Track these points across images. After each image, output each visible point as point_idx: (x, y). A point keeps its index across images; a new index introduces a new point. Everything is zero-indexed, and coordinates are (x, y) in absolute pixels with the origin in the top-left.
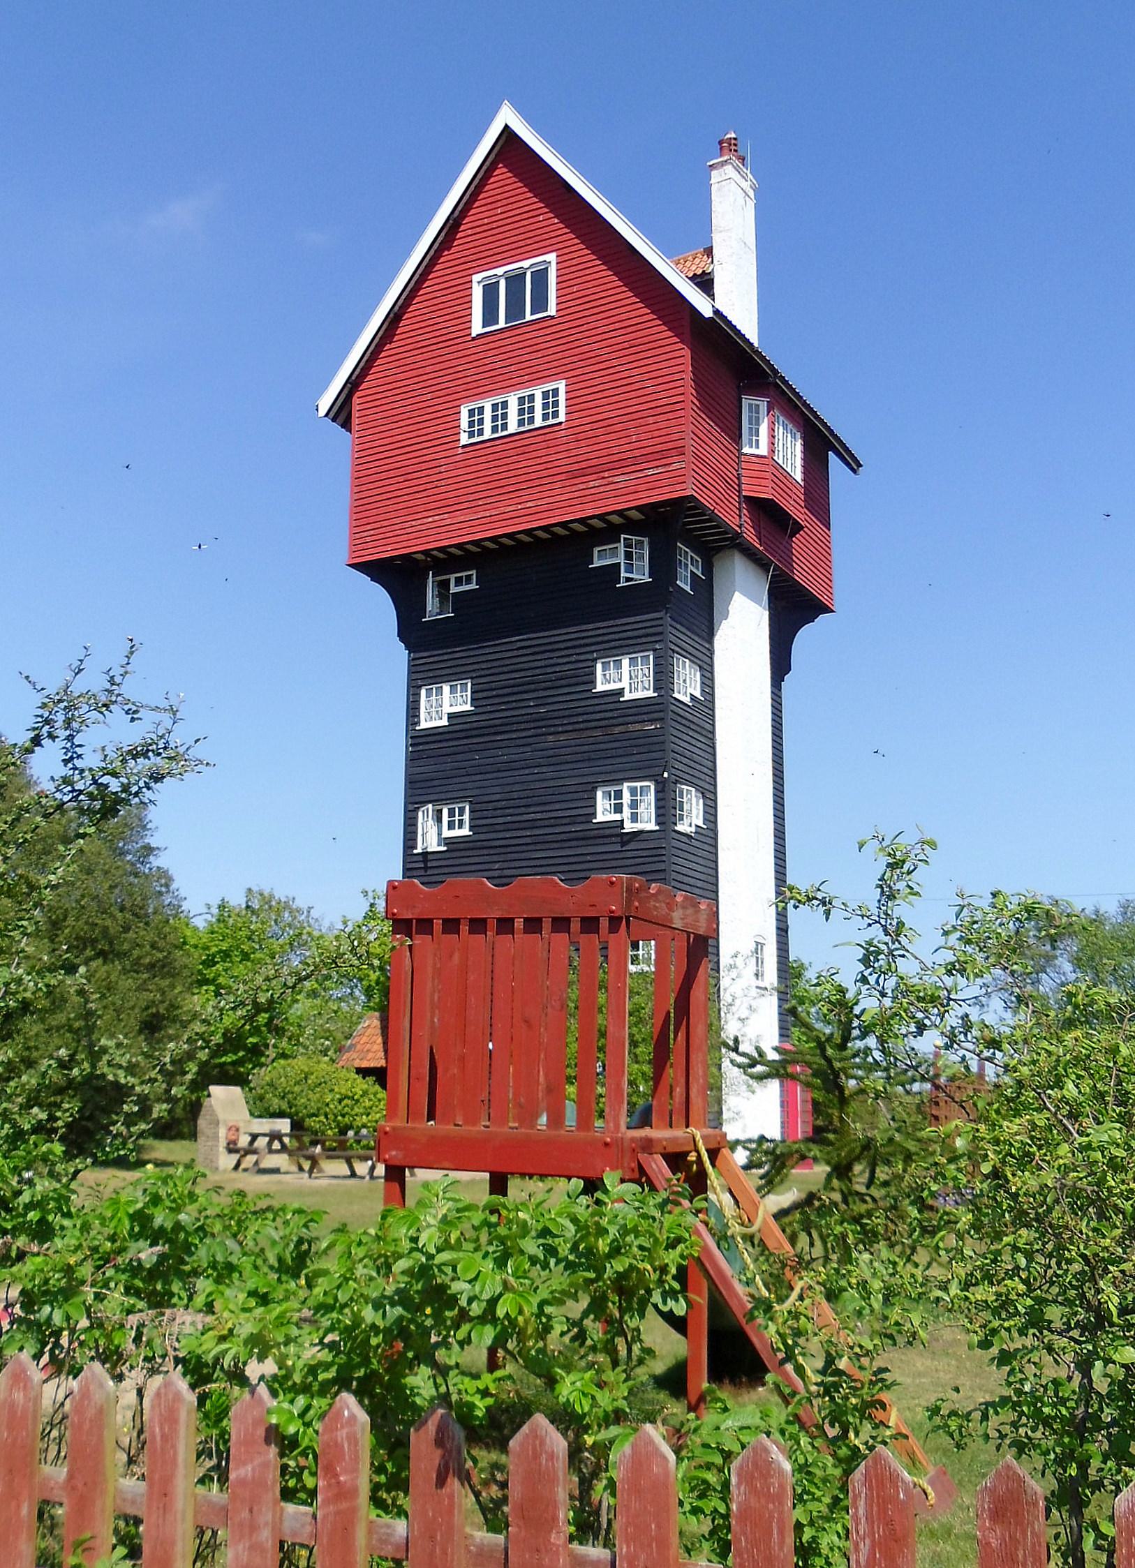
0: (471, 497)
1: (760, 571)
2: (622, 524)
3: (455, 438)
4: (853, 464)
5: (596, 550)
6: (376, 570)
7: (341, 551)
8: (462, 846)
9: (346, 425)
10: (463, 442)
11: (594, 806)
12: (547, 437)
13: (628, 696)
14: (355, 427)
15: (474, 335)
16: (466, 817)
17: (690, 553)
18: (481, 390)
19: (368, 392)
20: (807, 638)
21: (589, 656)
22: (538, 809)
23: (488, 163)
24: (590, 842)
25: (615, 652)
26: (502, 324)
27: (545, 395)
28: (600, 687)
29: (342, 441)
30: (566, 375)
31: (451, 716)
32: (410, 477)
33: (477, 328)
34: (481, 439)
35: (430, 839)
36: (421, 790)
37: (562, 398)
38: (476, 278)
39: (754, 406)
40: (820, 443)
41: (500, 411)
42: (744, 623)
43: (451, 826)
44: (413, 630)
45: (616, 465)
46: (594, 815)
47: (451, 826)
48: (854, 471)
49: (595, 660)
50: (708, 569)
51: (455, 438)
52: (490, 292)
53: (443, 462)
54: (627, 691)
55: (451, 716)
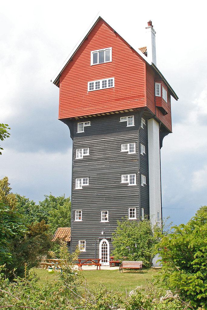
0: (91, 104)
1: (157, 123)
2: (123, 113)
3: (116, 79)
4: (176, 98)
5: (121, 118)
6: (64, 120)
7: (57, 117)
8: (87, 188)
9: (59, 87)
10: (88, 91)
11: (121, 179)
12: (110, 91)
13: (129, 153)
14: (60, 86)
15: (91, 65)
16: (88, 181)
17: (143, 119)
18: (98, 78)
19: (77, 64)
20: (166, 139)
21: (119, 143)
22: (106, 180)
23: (57, 79)
24: (120, 188)
25: (126, 142)
26: (98, 63)
27: (103, 82)
28: (123, 182)
29: (57, 90)
30: (115, 76)
31: (84, 156)
32: (74, 98)
33: (92, 64)
34: (93, 90)
35: (78, 187)
36: (75, 175)
37: (114, 81)
38: (92, 52)
39: (158, 85)
40: (171, 93)
41: (98, 84)
42: (154, 130)
43: (84, 183)
44: (73, 134)
45: (127, 98)
46: (121, 181)
47: (84, 183)
48: (177, 100)
49: (121, 144)
50: (146, 123)
51: (116, 79)
52: (95, 56)
53: (83, 95)
54: (129, 152)
55: (84, 156)
